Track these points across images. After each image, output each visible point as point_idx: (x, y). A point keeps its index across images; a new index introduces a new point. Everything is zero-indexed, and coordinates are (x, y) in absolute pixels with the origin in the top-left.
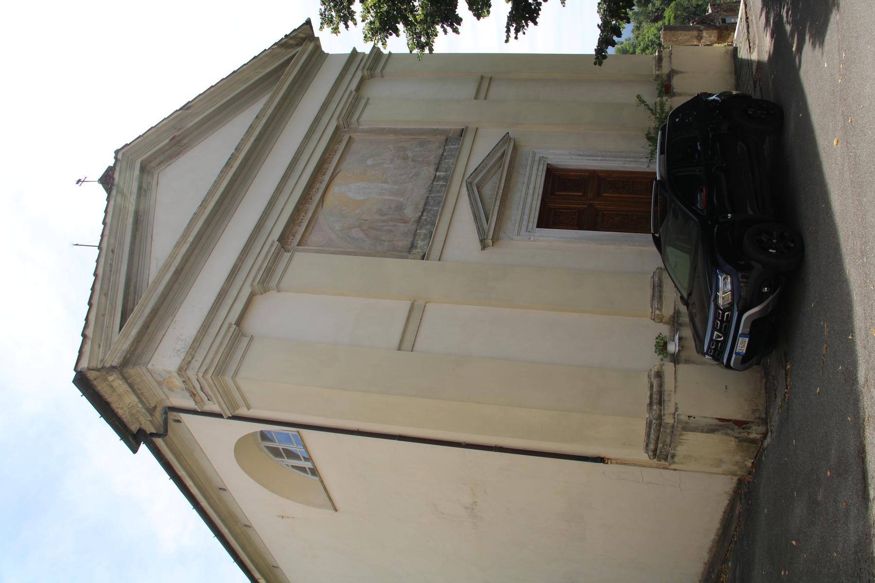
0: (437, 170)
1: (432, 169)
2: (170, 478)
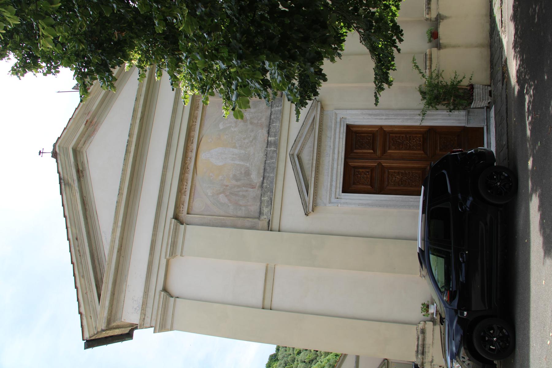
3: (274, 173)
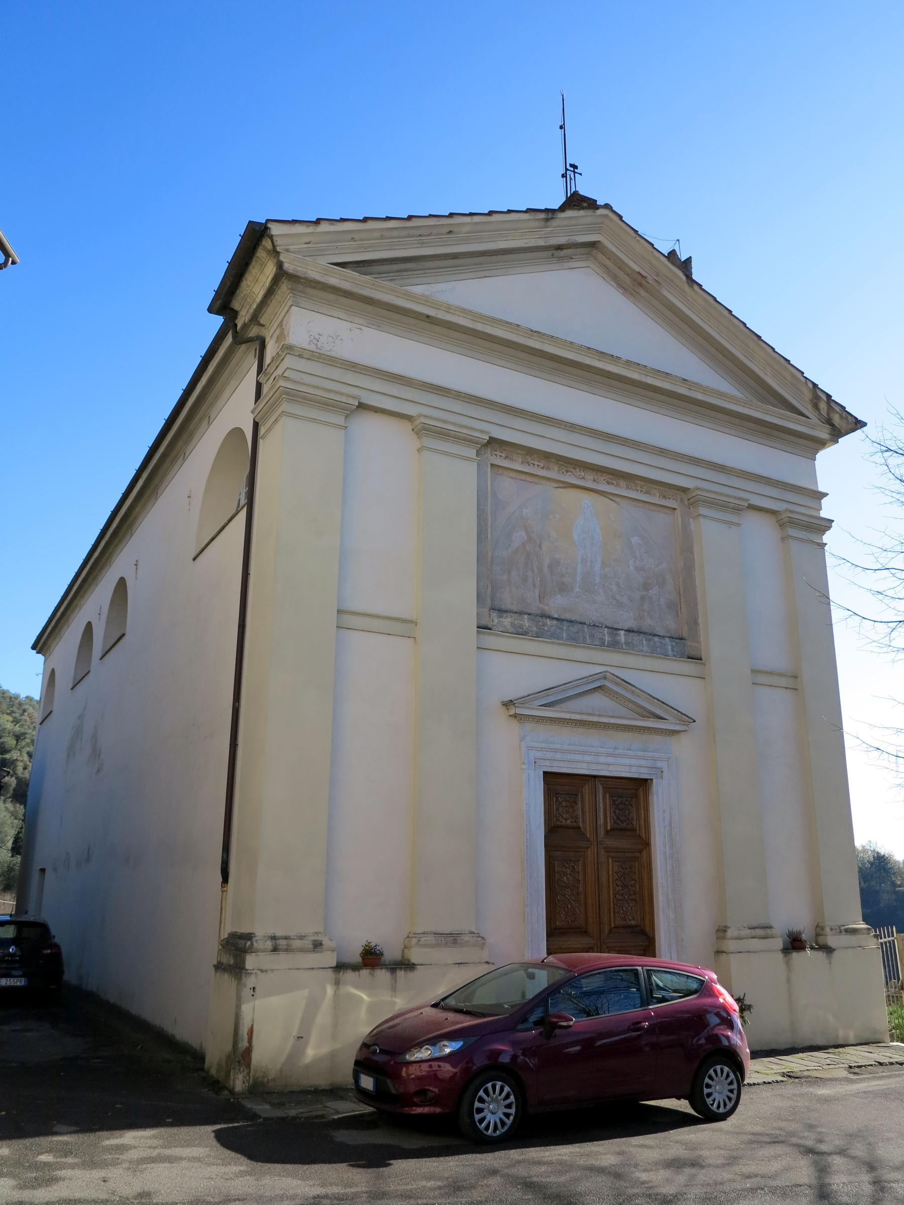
0: (629, 631)
1: (631, 624)
2: (203, 356)
3: (568, 639)
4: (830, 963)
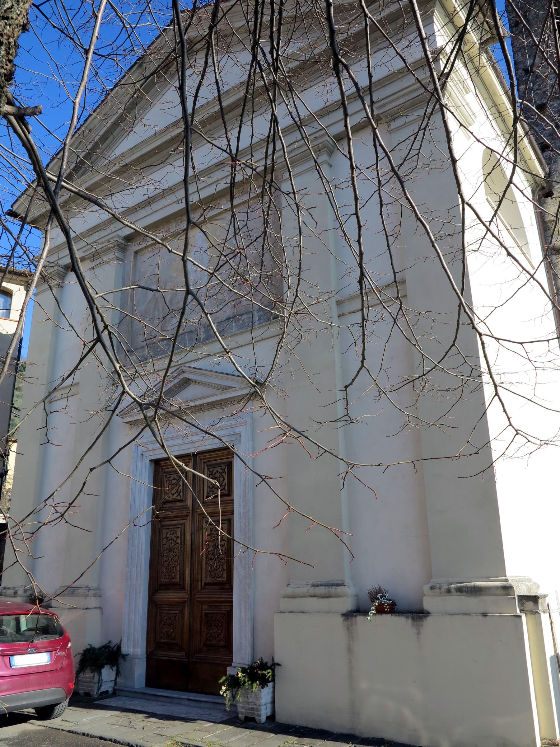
4: (419, 633)
